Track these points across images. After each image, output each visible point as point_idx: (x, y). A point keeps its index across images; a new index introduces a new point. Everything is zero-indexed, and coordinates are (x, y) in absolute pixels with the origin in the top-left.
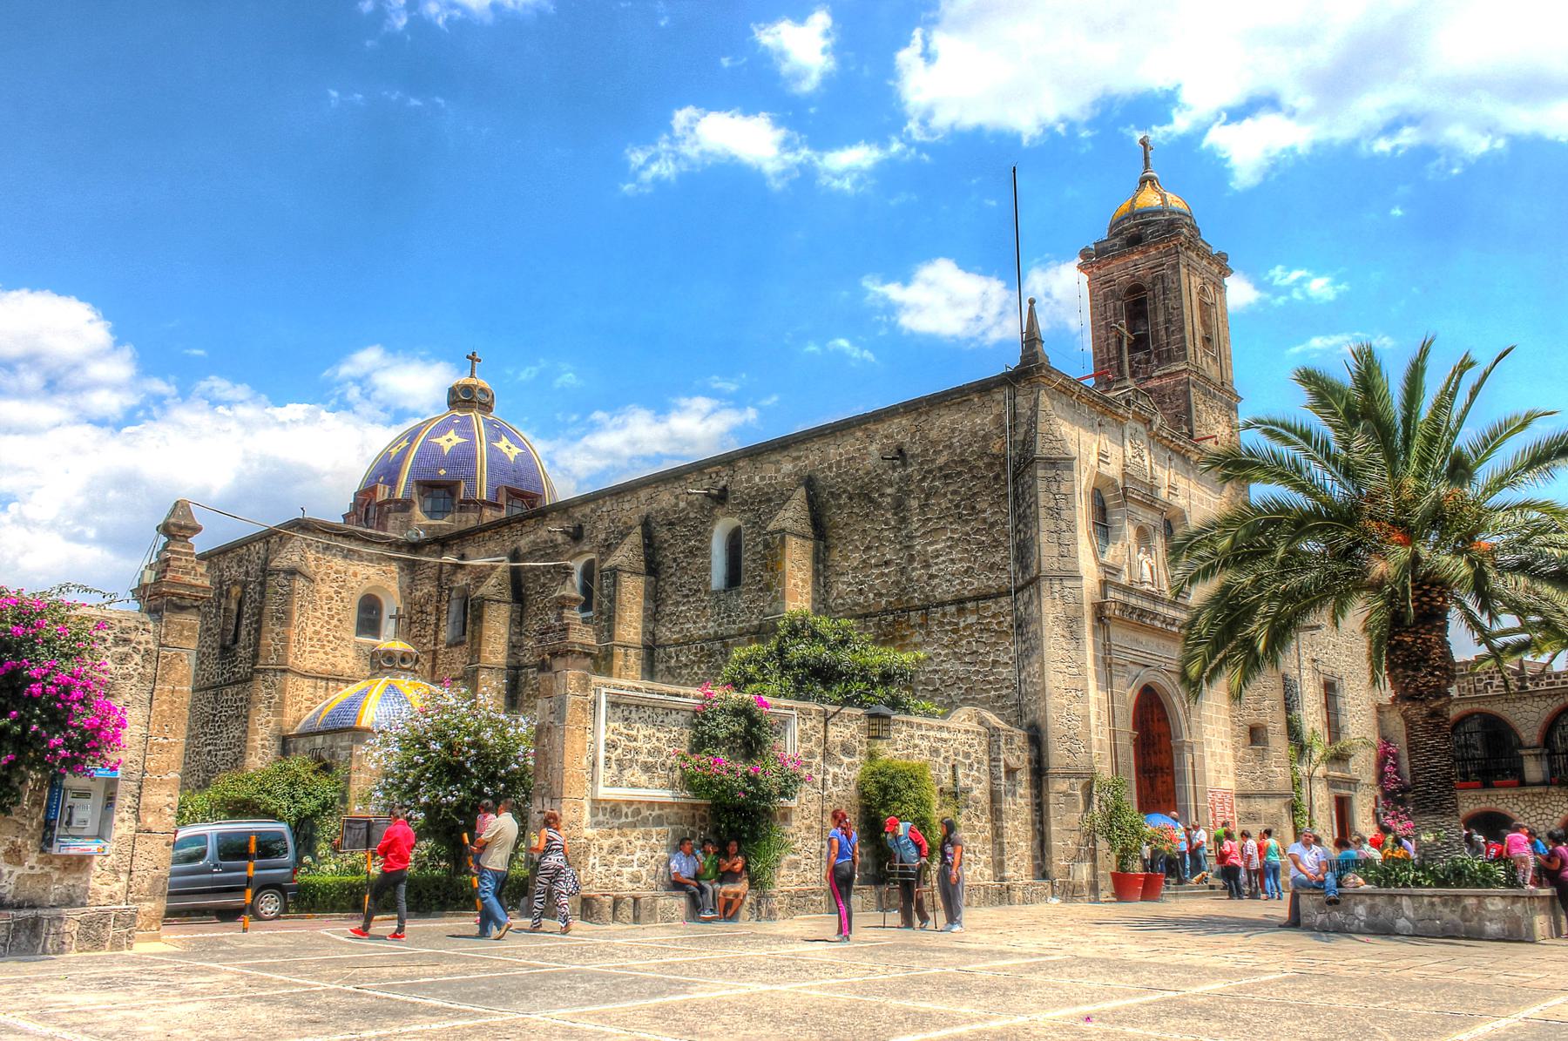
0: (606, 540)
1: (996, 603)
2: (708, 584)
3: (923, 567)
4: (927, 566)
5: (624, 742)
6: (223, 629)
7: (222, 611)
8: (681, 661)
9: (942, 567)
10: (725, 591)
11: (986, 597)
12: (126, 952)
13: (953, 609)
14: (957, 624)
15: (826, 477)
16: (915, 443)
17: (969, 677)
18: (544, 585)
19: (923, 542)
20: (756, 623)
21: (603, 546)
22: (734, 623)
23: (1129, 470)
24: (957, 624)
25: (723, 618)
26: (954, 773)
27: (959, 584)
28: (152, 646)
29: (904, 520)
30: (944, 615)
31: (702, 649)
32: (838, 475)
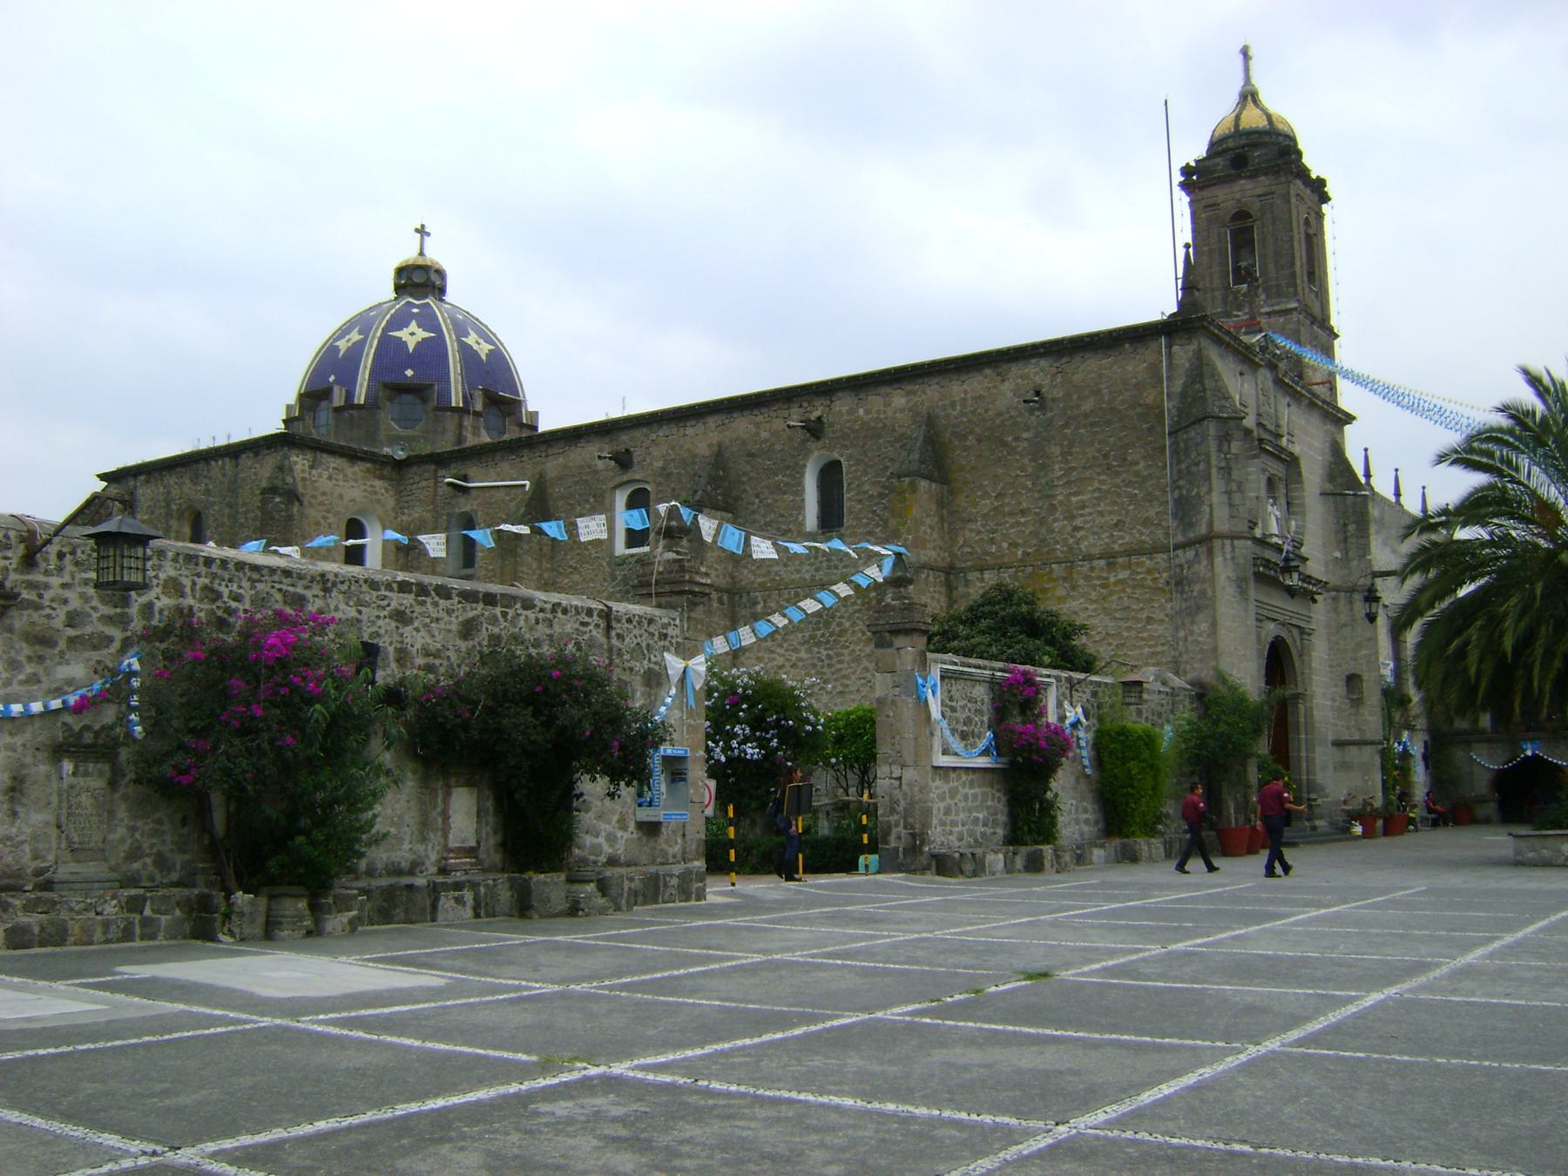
0: (664, 468)
2: (802, 524)
3: (1065, 518)
4: (1072, 517)
13: (1102, 563)
14: (1107, 578)
16: (1055, 386)
21: (661, 475)
22: (836, 567)
24: (1107, 578)
29: (1044, 467)
30: (1092, 569)
32: (962, 414)
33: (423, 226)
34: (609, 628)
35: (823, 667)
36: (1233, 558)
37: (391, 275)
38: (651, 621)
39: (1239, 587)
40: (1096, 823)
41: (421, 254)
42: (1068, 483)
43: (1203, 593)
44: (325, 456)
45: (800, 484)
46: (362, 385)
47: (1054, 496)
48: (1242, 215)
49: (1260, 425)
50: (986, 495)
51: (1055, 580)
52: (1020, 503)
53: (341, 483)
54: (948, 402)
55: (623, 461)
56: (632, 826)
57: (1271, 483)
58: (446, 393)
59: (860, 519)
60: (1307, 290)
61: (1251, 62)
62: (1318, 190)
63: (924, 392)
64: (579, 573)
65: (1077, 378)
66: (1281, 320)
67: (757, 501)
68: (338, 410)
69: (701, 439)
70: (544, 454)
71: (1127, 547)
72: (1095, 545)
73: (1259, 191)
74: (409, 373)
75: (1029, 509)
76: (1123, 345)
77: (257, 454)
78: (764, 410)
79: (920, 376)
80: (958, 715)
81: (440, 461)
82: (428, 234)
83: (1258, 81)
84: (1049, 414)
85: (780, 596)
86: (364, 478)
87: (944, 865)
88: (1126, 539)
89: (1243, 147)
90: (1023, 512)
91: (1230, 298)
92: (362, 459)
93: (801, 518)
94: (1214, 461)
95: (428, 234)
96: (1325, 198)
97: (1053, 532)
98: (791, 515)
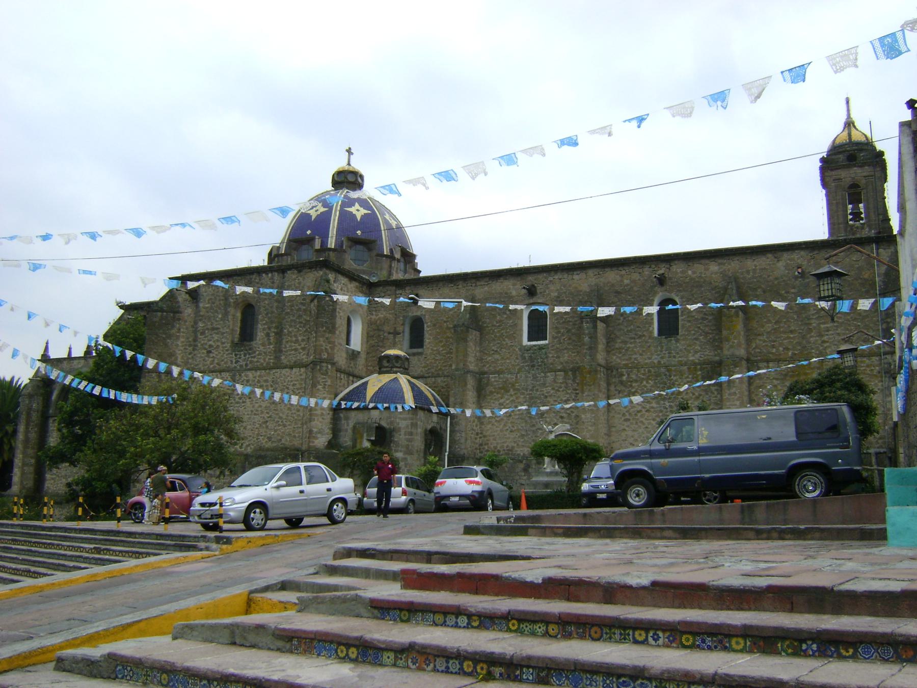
3: (818, 336)
4: (821, 335)
16: (810, 266)
18: (500, 321)
22: (674, 357)
33: (350, 148)
35: (667, 412)
41: (349, 164)
44: (340, 276)
47: (810, 324)
48: (854, 186)
50: (769, 321)
52: (789, 327)
54: (745, 270)
64: (500, 354)
67: (622, 318)
68: (317, 251)
70: (474, 285)
73: (865, 174)
74: (359, 232)
75: (795, 330)
77: (300, 271)
79: (728, 255)
83: (853, 116)
85: (638, 371)
89: (854, 150)
90: (791, 332)
91: (849, 229)
93: (651, 329)
95: (352, 154)
97: (810, 343)
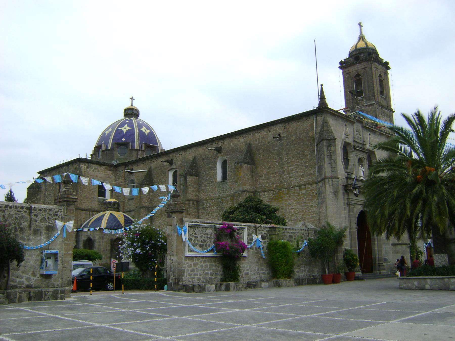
0: (181, 164)
1: (312, 186)
2: (216, 179)
3: (288, 174)
4: (289, 174)
5: (194, 238)
6: (55, 195)
7: (54, 189)
8: (207, 205)
9: (294, 174)
10: (222, 182)
11: (308, 184)
12: (64, 300)
13: (298, 188)
14: (299, 193)
15: (255, 144)
16: (284, 132)
17: (303, 211)
18: (160, 179)
19: (287, 166)
20: (232, 192)
21: (180, 166)
22: (225, 192)
23: (355, 140)
25: (221, 191)
26: (298, 243)
27: (299, 180)
28: (63, 216)
29: (281, 158)
30: (295, 190)
31: (215, 201)
32: (259, 143)
33: (132, 97)
34: (30, 213)
36: (332, 185)
37: (123, 111)
38: (50, 210)
39: (335, 194)
40: (268, 274)
41: (132, 105)
42: (288, 163)
43: (324, 197)
44: (91, 164)
45: (216, 167)
46: (110, 144)
48: (358, 75)
49: (354, 141)
50: (265, 168)
51: (284, 194)
52: (274, 170)
53: (97, 172)
54: (255, 139)
55: (170, 162)
56: (38, 275)
57: (360, 160)
58: (133, 145)
59: (231, 177)
60: (380, 97)
61: (362, 28)
62: (386, 66)
63: (248, 137)
65: (290, 130)
66: (371, 107)
68: (103, 151)
69: (190, 155)
71: (305, 183)
72: (296, 182)
73: (362, 67)
76: (302, 118)
77: (73, 165)
78: (206, 145)
80: (199, 239)
81: (126, 165)
82: (134, 99)
84: (282, 142)
85: (210, 202)
86: (104, 171)
87: (189, 289)
88: (304, 180)
89: (358, 54)
92: (104, 165)
94: (325, 154)
96: (389, 68)
98: (213, 177)
